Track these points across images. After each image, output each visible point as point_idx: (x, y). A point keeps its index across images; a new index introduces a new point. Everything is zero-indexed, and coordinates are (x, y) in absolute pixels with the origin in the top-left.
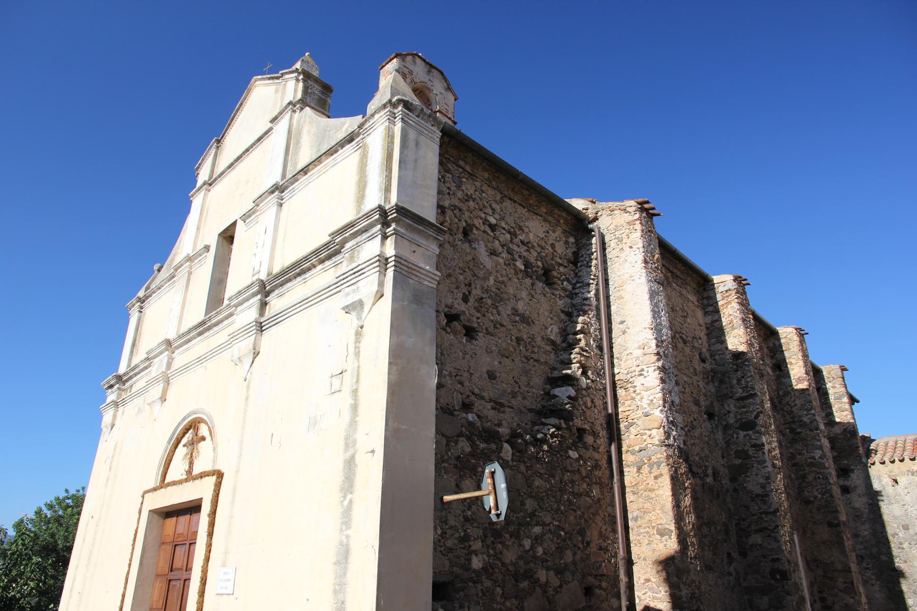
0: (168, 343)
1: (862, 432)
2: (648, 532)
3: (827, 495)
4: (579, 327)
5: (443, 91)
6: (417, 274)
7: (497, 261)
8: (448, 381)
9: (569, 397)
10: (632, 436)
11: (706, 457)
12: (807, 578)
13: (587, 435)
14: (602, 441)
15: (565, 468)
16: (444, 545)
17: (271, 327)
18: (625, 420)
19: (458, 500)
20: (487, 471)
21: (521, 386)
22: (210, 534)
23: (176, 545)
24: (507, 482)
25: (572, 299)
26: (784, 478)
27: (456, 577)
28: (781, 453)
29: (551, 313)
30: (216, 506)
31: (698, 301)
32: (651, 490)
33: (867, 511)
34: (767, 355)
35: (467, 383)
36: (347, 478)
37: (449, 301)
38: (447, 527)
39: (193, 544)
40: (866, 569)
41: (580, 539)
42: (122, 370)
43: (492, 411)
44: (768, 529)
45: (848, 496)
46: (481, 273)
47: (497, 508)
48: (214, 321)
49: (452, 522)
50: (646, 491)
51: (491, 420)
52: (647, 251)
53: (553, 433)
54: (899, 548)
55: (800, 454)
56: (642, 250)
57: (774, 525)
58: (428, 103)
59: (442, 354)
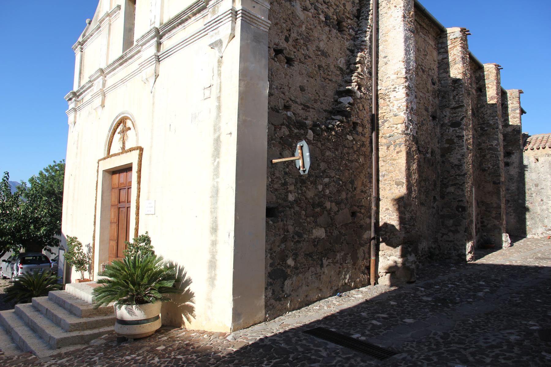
0: (102, 71)
1: (524, 131)
2: (390, 183)
3: (496, 166)
4: (358, 60)
6: (256, 22)
7: (308, 14)
8: (275, 92)
9: (349, 103)
10: (386, 128)
11: (428, 142)
12: (476, 211)
13: (358, 127)
14: (367, 130)
15: (344, 145)
16: (273, 187)
17: (164, 58)
18: (382, 118)
19: (281, 162)
20: (298, 145)
21: (321, 96)
22: (139, 183)
23: (120, 189)
24: (310, 152)
25: (355, 41)
26: (472, 156)
27: (279, 205)
28: (473, 142)
29: (341, 50)
30: (141, 167)
31: (435, 45)
32: (394, 160)
33: (517, 176)
34: (474, 82)
35: (287, 93)
36: (216, 149)
38: (274, 177)
39: (130, 188)
40: (509, 207)
41: (351, 186)
42: (75, 89)
43: (302, 111)
44: (458, 184)
45: (508, 167)
46: (297, 22)
47: (304, 167)
48: (128, 56)
49: (277, 174)
50: (391, 160)
51: (301, 116)
52: (406, 9)
53: (338, 124)
54: (530, 196)
55: (484, 143)
56: (403, 8)
57: (462, 182)
59: (272, 75)
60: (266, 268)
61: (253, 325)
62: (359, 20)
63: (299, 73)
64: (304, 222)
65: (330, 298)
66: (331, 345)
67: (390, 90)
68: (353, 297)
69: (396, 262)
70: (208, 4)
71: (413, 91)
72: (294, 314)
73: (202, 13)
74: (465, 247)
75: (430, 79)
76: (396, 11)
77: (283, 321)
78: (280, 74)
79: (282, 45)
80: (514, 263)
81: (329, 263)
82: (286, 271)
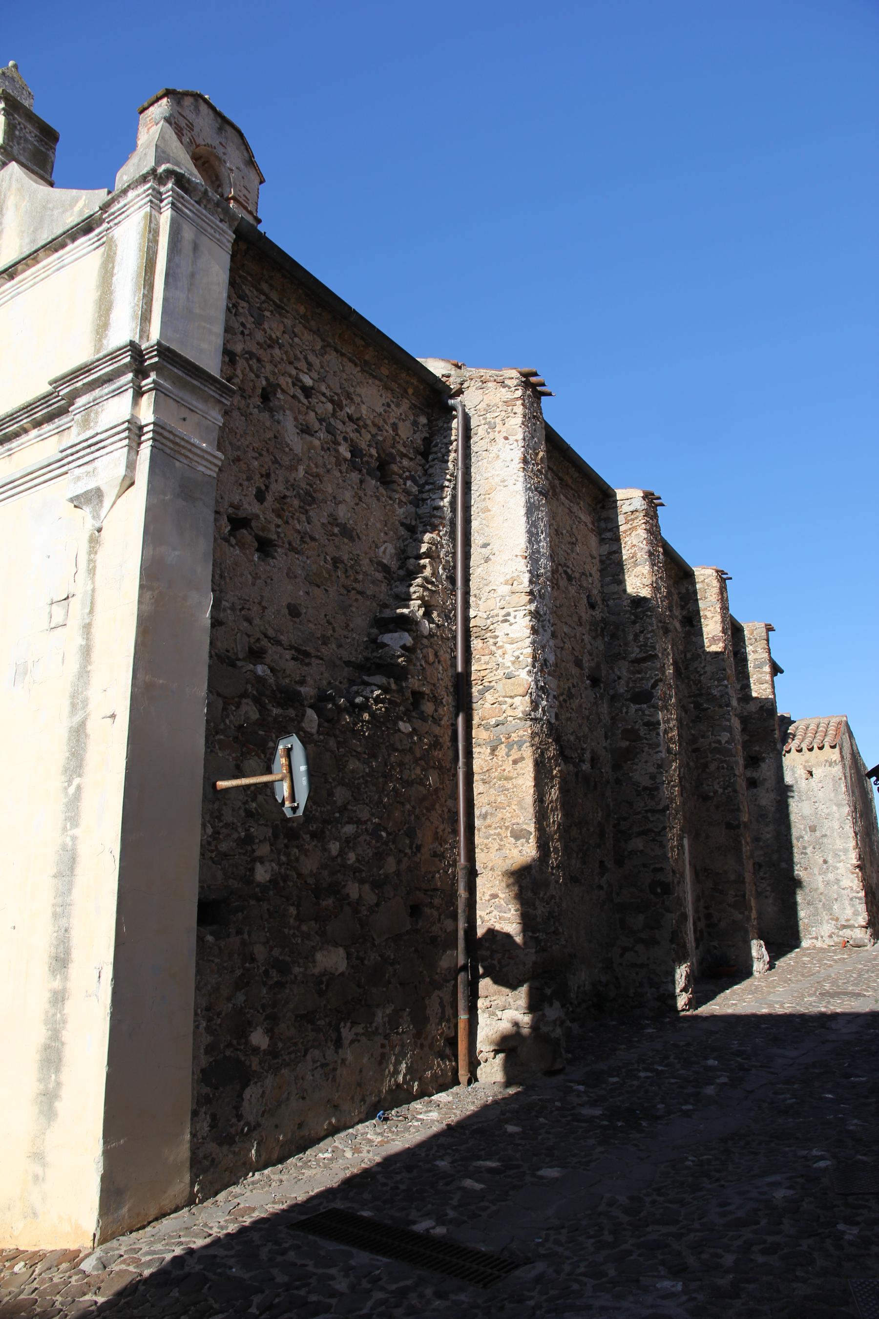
1: (781, 711)
2: (499, 834)
3: (730, 789)
4: (424, 548)
5: (242, 166)
7: (311, 442)
8: (228, 616)
9: (404, 647)
10: (487, 705)
11: (584, 736)
14: (446, 710)
16: (217, 849)
18: (479, 682)
20: (281, 747)
21: (337, 629)
25: (417, 506)
26: (680, 767)
29: (386, 525)
31: (593, 523)
32: (508, 779)
33: (773, 809)
35: (257, 621)
36: (73, 754)
37: (236, 499)
38: (221, 824)
40: (763, 878)
41: (408, 842)
43: (293, 663)
45: (755, 790)
49: (228, 817)
50: (500, 780)
51: (290, 676)
52: (529, 446)
54: (802, 853)
55: (703, 737)
56: (521, 443)
58: (218, 183)
59: (222, 576)
60: (195, 1057)
61: (156, 1219)
62: (428, 462)
63: (287, 575)
64: (294, 936)
65: (360, 1126)
66: (362, 1258)
67: (496, 619)
68: (418, 1120)
69: (516, 1024)
70: (73, 404)
71: (546, 623)
72: (268, 1177)
73: (57, 422)
74: (674, 976)
75: (584, 597)
76: (508, 447)
77: (237, 1200)
78: (242, 575)
79: (249, 508)
80: (779, 1010)
81: (356, 1034)
82: (247, 1063)
